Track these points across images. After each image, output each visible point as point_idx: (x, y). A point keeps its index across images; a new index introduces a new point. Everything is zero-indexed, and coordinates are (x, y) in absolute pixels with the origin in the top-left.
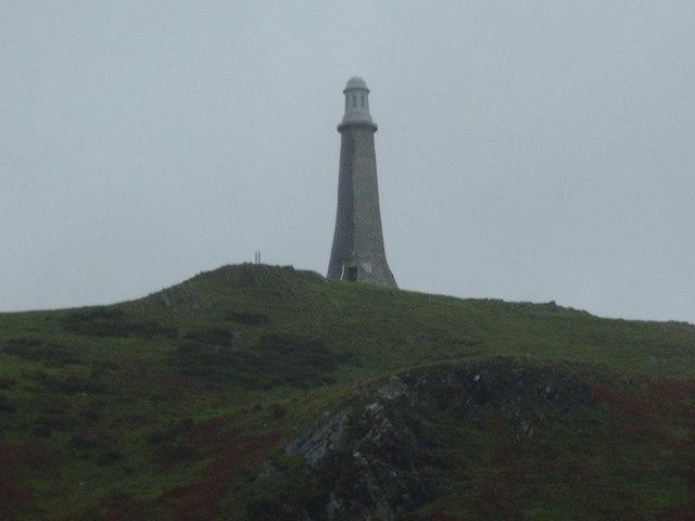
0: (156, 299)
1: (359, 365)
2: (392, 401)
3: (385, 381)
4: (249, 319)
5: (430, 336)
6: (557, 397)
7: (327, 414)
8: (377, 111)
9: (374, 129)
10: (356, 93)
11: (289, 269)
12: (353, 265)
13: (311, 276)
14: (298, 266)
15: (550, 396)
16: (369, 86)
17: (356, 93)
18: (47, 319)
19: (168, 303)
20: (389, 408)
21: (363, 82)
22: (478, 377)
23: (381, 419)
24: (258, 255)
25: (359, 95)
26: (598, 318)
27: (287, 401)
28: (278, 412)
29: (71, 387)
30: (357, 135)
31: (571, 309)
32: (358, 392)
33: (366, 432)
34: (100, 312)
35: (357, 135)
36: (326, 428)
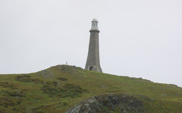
0: (39, 73)
1: (89, 92)
2: (92, 103)
3: (91, 98)
4: (62, 79)
5: (108, 86)
6: (134, 104)
7: (76, 105)
8: (99, 28)
9: (99, 32)
10: (95, 23)
11: (74, 67)
12: (92, 66)
13: (80, 69)
14: (144, 78)
15: (132, 104)
16: (98, 21)
17: (95, 23)
18: (12, 77)
19: (42, 74)
20: (91, 105)
21: (96, 20)
22: (114, 98)
23: (88, 108)
24: (67, 63)
25: (95, 23)
26: (152, 83)
27: (68, 101)
28: (65, 104)
29: (14, 95)
30: (94, 33)
31: (146, 80)
32: (84, 100)
33: (85, 110)
34: (25, 75)
35: (94, 33)
36: (75, 109)
